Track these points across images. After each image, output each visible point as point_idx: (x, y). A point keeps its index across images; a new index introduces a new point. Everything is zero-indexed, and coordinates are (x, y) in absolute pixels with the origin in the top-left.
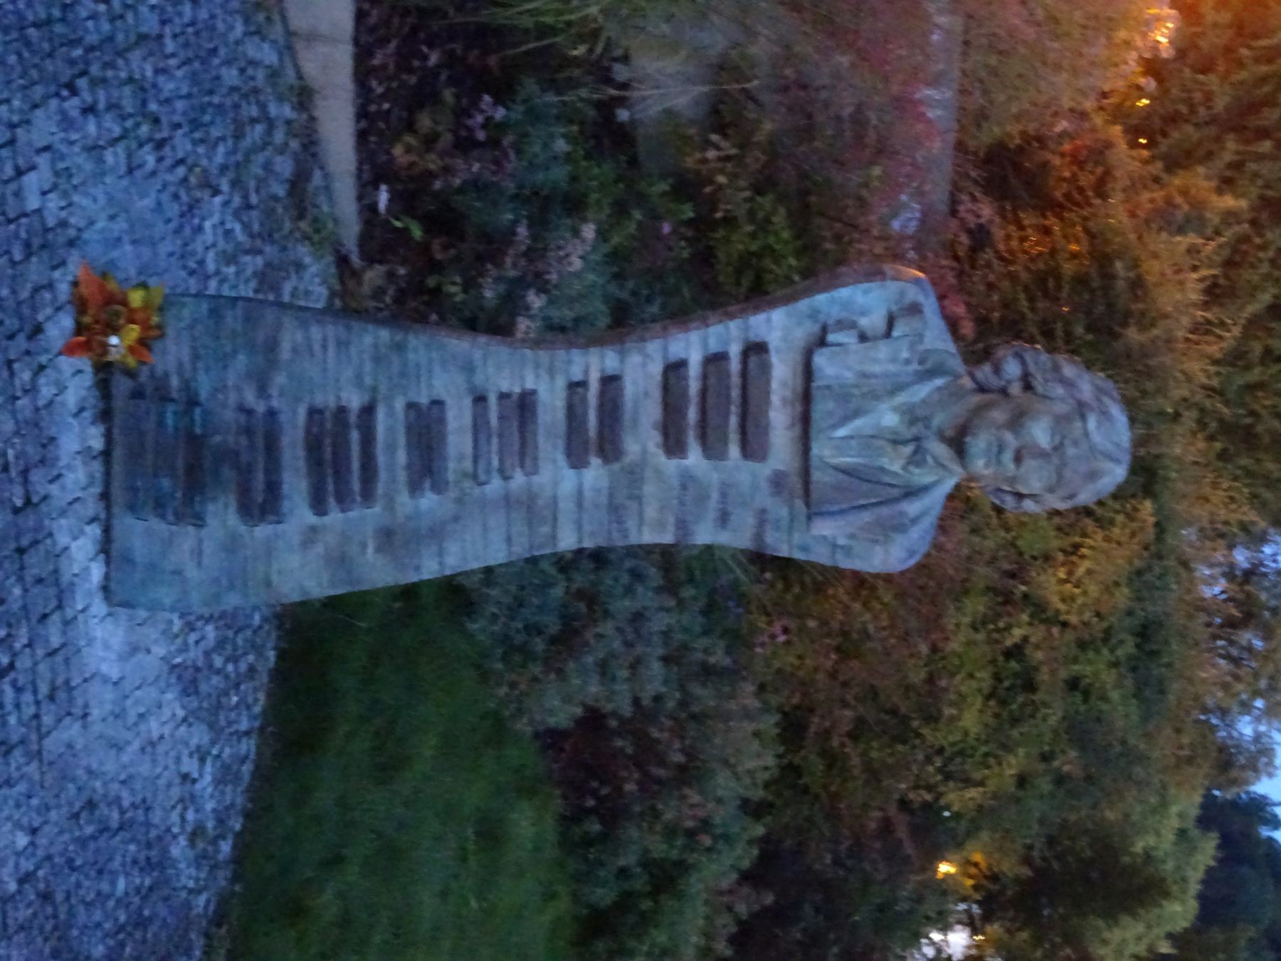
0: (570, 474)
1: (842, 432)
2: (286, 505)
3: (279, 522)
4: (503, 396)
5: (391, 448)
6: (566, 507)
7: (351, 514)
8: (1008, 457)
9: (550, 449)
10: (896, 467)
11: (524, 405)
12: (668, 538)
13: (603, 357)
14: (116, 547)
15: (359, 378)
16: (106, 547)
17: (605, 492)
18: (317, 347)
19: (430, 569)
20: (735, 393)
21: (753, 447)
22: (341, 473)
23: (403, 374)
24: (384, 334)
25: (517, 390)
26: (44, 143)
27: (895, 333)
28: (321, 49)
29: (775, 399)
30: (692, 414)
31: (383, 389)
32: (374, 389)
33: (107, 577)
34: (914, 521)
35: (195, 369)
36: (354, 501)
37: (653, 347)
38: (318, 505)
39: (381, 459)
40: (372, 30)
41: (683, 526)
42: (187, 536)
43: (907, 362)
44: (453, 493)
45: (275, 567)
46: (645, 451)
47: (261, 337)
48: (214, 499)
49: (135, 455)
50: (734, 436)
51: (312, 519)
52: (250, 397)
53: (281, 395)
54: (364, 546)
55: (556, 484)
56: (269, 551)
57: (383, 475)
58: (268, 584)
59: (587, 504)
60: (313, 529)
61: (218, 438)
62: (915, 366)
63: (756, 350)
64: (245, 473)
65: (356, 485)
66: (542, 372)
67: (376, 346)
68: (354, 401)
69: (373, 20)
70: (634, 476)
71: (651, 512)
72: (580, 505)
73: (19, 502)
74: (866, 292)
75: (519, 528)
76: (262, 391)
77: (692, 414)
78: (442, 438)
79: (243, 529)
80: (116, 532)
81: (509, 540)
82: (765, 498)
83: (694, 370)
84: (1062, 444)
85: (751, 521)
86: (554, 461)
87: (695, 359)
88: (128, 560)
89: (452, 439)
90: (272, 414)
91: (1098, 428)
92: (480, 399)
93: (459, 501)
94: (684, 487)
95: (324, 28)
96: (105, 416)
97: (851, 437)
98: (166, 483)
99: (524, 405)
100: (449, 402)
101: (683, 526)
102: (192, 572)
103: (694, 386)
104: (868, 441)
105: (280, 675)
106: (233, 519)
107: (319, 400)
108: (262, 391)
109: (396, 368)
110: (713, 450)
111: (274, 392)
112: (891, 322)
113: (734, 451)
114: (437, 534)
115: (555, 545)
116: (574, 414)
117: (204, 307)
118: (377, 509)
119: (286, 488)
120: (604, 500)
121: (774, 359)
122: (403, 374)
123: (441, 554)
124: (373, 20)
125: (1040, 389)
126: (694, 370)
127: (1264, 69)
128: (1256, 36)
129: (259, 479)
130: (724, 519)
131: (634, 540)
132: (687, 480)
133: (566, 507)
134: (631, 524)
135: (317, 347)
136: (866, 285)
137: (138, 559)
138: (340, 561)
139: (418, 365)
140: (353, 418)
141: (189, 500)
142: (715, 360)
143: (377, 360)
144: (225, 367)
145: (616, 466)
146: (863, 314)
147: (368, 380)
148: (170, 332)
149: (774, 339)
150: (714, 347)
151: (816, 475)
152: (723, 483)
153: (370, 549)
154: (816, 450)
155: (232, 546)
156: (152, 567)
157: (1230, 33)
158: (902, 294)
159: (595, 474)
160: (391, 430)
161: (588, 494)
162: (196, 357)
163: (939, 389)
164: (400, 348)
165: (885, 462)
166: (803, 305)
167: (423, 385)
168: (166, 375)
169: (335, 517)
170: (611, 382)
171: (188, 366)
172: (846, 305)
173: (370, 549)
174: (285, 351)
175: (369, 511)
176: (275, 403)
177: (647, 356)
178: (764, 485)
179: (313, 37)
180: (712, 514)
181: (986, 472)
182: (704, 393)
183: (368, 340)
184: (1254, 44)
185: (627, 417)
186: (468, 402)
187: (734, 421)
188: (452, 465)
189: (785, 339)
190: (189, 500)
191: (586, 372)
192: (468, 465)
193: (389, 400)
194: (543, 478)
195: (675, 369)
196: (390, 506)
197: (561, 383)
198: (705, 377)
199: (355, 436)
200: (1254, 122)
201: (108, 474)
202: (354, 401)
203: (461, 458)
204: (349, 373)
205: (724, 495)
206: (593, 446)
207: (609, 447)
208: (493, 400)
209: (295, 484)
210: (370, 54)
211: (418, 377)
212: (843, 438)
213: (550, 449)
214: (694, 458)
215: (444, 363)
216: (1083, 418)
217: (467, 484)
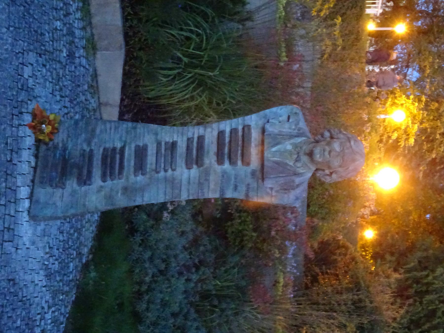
0: (186, 171)
1: (274, 149)
2: (93, 180)
3: (90, 185)
4: (166, 143)
5: (129, 161)
6: (184, 182)
7: (115, 182)
8: (326, 153)
9: (180, 162)
10: (291, 164)
11: (174, 145)
12: (217, 196)
13: (199, 129)
14: (34, 198)
15: (121, 138)
16: (31, 197)
17: (197, 178)
18: (108, 130)
19: (139, 202)
20: (240, 143)
21: (246, 163)
22: (112, 168)
23: (135, 137)
24: (130, 124)
25: (171, 141)
26: (32, 63)
27: (290, 121)
28: (109, 109)
29: (253, 145)
30: (226, 150)
31: (128, 141)
32: (125, 142)
33: (30, 207)
34: (298, 186)
35: (67, 141)
36: (115, 177)
37: (215, 125)
38: (104, 178)
39: (126, 164)
40: (125, 106)
41: (222, 191)
42: (59, 192)
43: (294, 130)
44: (148, 176)
45: (87, 199)
46: (211, 163)
47: (90, 128)
48: (69, 180)
49: (45, 166)
50: (239, 158)
51: (102, 184)
52: (85, 147)
53: (95, 145)
54: (117, 192)
55: (182, 175)
56: (86, 194)
57: (126, 169)
58: (84, 205)
59: (191, 182)
60: (102, 187)
61: (73, 161)
62: (296, 131)
63: (247, 128)
64: (80, 169)
65: (117, 171)
66: (179, 135)
67: (127, 128)
68: (119, 145)
69: (125, 103)
70: (207, 173)
71: (212, 186)
72: (189, 183)
73: (9, 159)
74: (281, 109)
75: (169, 190)
76: (89, 144)
77: (226, 150)
78: (146, 156)
79: (78, 188)
80: (35, 191)
81: (165, 194)
82: (249, 180)
83: (227, 135)
84: (343, 149)
85: (244, 189)
86: (182, 167)
87: (228, 130)
88: (37, 202)
89: (149, 162)
90: (91, 151)
91: (354, 144)
92: (159, 144)
93: (150, 178)
94: (223, 176)
95: (111, 102)
96: (36, 156)
97: (276, 151)
98: (54, 174)
99: (174, 145)
100: (149, 145)
101: (222, 191)
102: (59, 204)
103: (227, 140)
104: (281, 153)
105: (76, 303)
106: (75, 185)
107: (107, 146)
108: (89, 144)
109: (133, 135)
110: (232, 162)
111: (93, 144)
112: (289, 118)
113: (239, 163)
114: (142, 189)
115: (180, 198)
116: (189, 148)
117: (73, 122)
118: (123, 180)
119: (94, 174)
120: (197, 181)
121: (253, 131)
122: (135, 137)
123: (143, 196)
124: (125, 103)
125: (335, 137)
126: (227, 135)
127: (408, 275)
128: (405, 265)
129: (85, 172)
130: (236, 188)
131: (206, 196)
132: (224, 173)
133: (184, 182)
134: (205, 190)
135: (108, 130)
136: (281, 107)
137: (41, 201)
138: (109, 198)
139: (140, 134)
140: (118, 151)
141: (61, 178)
142: (234, 131)
143: (127, 132)
144: (78, 138)
145: (201, 168)
146: (280, 116)
147: (124, 139)
148: (61, 131)
149: (253, 124)
150: (234, 126)
151: (266, 163)
152: (235, 175)
153: (120, 194)
154: (266, 155)
155: (73, 193)
156: (47, 203)
157: (395, 264)
158: (292, 109)
159: (194, 171)
160: (130, 155)
161: (192, 179)
162: (69, 136)
163: (304, 140)
164: (135, 128)
165: (288, 161)
166: (262, 113)
167: (141, 140)
168: (58, 143)
169: (109, 182)
170: (201, 139)
171: (65, 140)
172: (275, 113)
173: (120, 194)
174: (98, 131)
175: (120, 181)
176: (93, 148)
177: (212, 129)
178: (249, 176)
179: (106, 104)
180: (232, 187)
181: (320, 160)
182: (230, 142)
183: (125, 126)
184: (404, 267)
185: (206, 150)
186: (155, 145)
187: (240, 152)
188: (148, 166)
189: (256, 124)
190: (61, 178)
191: (193, 134)
192: (154, 166)
193: (130, 143)
194: (177, 173)
195: (221, 134)
196: (127, 178)
197: (185, 139)
198: (231, 137)
199: (118, 156)
200: (406, 293)
201: (34, 176)
202: (119, 145)
203: (151, 164)
204: (118, 136)
205: (236, 178)
206: (194, 162)
207: (199, 162)
208: (163, 143)
209: (97, 172)
210: (124, 115)
211: (140, 137)
212: (274, 151)
213: (180, 162)
214: (227, 166)
215: (148, 132)
216: (350, 142)
217: (153, 173)
